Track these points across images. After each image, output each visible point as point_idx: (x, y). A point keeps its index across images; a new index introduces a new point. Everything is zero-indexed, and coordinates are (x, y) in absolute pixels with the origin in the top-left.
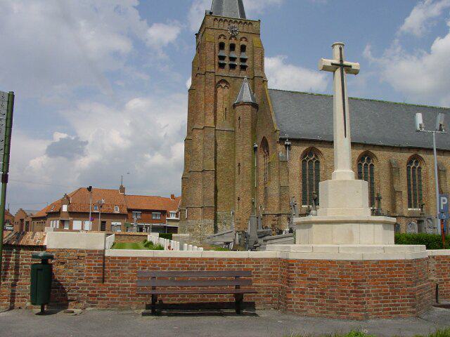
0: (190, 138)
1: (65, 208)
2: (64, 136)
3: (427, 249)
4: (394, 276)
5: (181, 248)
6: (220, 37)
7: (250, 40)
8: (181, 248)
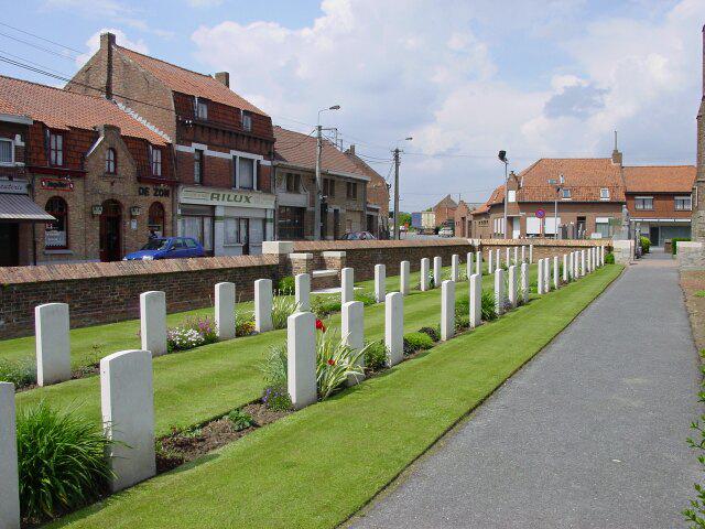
1: (512, 197)
2: (571, 81)
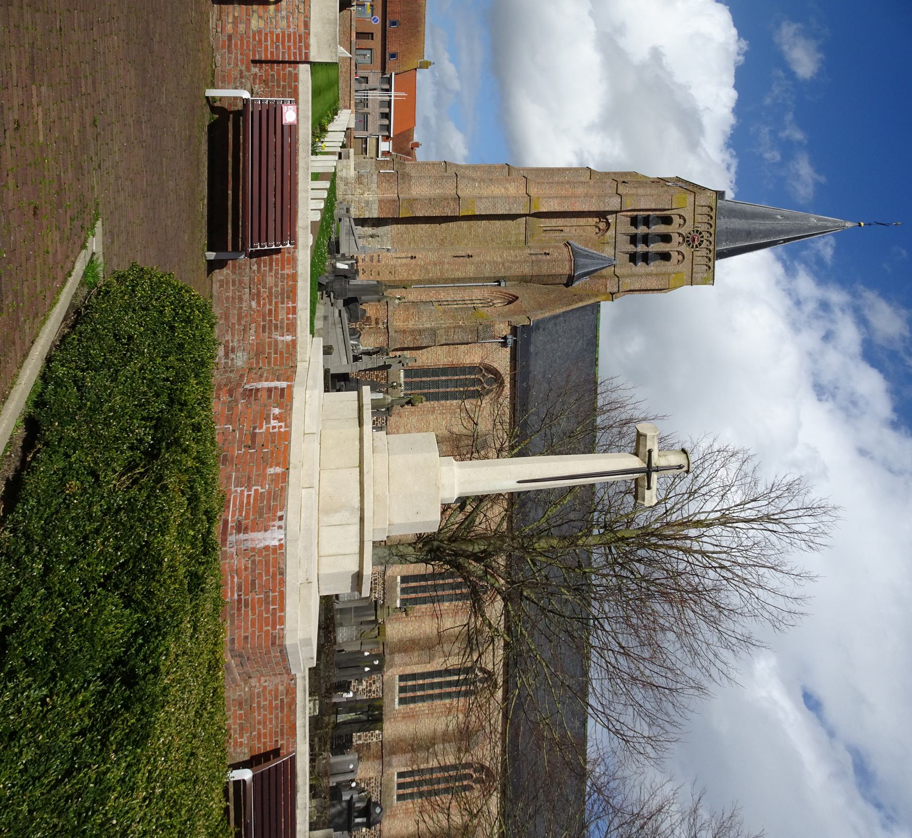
0: (514, 173)
3: (310, 669)
4: (253, 609)
5: (316, 177)
6: (680, 216)
7: (680, 267)
8: (316, 177)
